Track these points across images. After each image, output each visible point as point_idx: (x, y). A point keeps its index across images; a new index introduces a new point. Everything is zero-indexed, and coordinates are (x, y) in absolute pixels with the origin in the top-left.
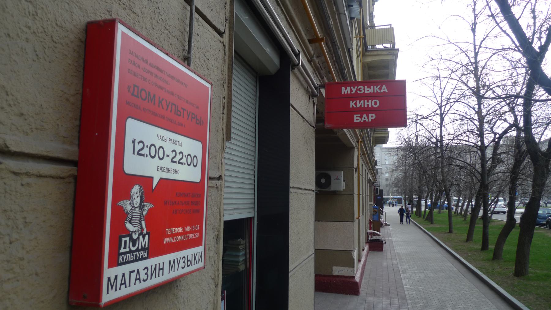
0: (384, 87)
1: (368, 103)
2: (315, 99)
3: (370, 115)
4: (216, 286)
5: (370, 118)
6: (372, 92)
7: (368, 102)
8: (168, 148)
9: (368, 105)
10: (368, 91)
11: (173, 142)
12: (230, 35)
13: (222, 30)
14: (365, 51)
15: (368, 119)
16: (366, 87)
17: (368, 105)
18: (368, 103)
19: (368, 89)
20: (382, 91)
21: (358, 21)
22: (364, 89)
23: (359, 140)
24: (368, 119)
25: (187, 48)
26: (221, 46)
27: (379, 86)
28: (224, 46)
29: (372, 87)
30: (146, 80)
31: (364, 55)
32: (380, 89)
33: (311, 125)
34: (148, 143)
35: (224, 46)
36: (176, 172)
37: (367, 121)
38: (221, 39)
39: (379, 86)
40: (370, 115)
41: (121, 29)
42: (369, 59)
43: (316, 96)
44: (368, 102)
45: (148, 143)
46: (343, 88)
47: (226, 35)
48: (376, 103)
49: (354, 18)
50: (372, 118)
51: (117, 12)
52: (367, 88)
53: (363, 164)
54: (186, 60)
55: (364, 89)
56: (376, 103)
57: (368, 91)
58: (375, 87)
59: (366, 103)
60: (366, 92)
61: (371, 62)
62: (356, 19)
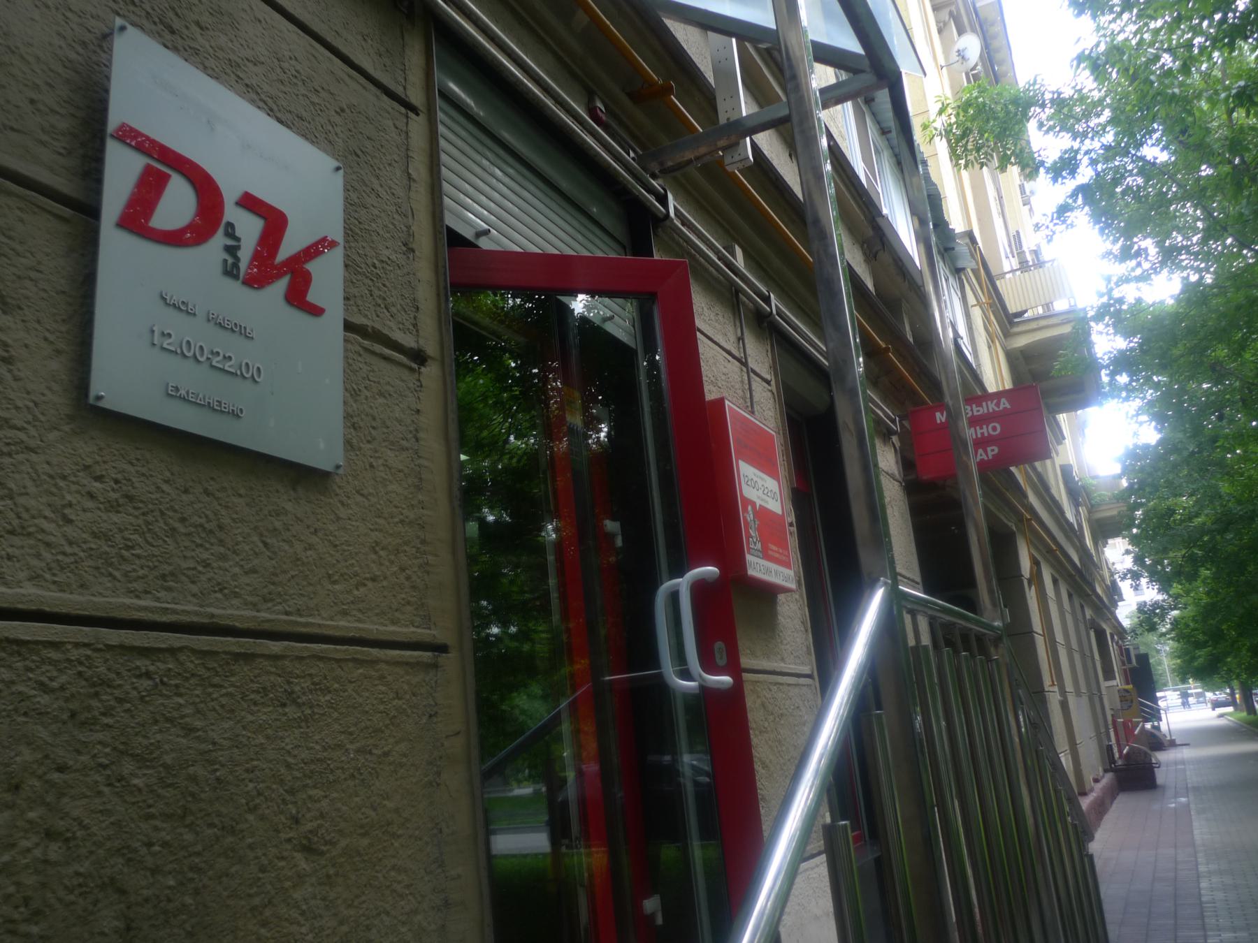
0: (1003, 400)
1: (982, 431)
2: (895, 439)
3: (989, 449)
4: (806, 631)
5: (990, 454)
6: (986, 411)
7: (981, 428)
8: (760, 483)
9: (982, 434)
10: (978, 411)
11: (762, 479)
12: (777, 382)
13: (769, 379)
14: (1008, 326)
15: (987, 456)
16: (974, 406)
17: (982, 434)
18: (982, 431)
19: (978, 408)
20: (1001, 408)
21: (976, 272)
22: (972, 410)
23: (1022, 515)
24: (987, 456)
25: (749, 404)
26: (769, 394)
27: (995, 401)
28: (773, 394)
29: (984, 404)
30: (103, 571)
31: (1007, 334)
32: (998, 405)
33: (894, 480)
34: (750, 478)
35: (773, 394)
36: (767, 502)
37: (986, 458)
38: (769, 388)
39: (995, 401)
40: (989, 449)
41: (727, 403)
42: (1021, 342)
43: (895, 433)
44: (981, 428)
45: (750, 478)
46: (938, 415)
47: (773, 383)
48: (994, 429)
49: (963, 269)
50: (993, 453)
51: (725, 394)
52: (977, 407)
53: (1039, 557)
54: (752, 412)
55: (972, 410)
56: (994, 429)
57: (978, 411)
58: (989, 403)
59: (979, 432)
60: (975, 413)
61: (1028, 346)
62: (969, 270)
